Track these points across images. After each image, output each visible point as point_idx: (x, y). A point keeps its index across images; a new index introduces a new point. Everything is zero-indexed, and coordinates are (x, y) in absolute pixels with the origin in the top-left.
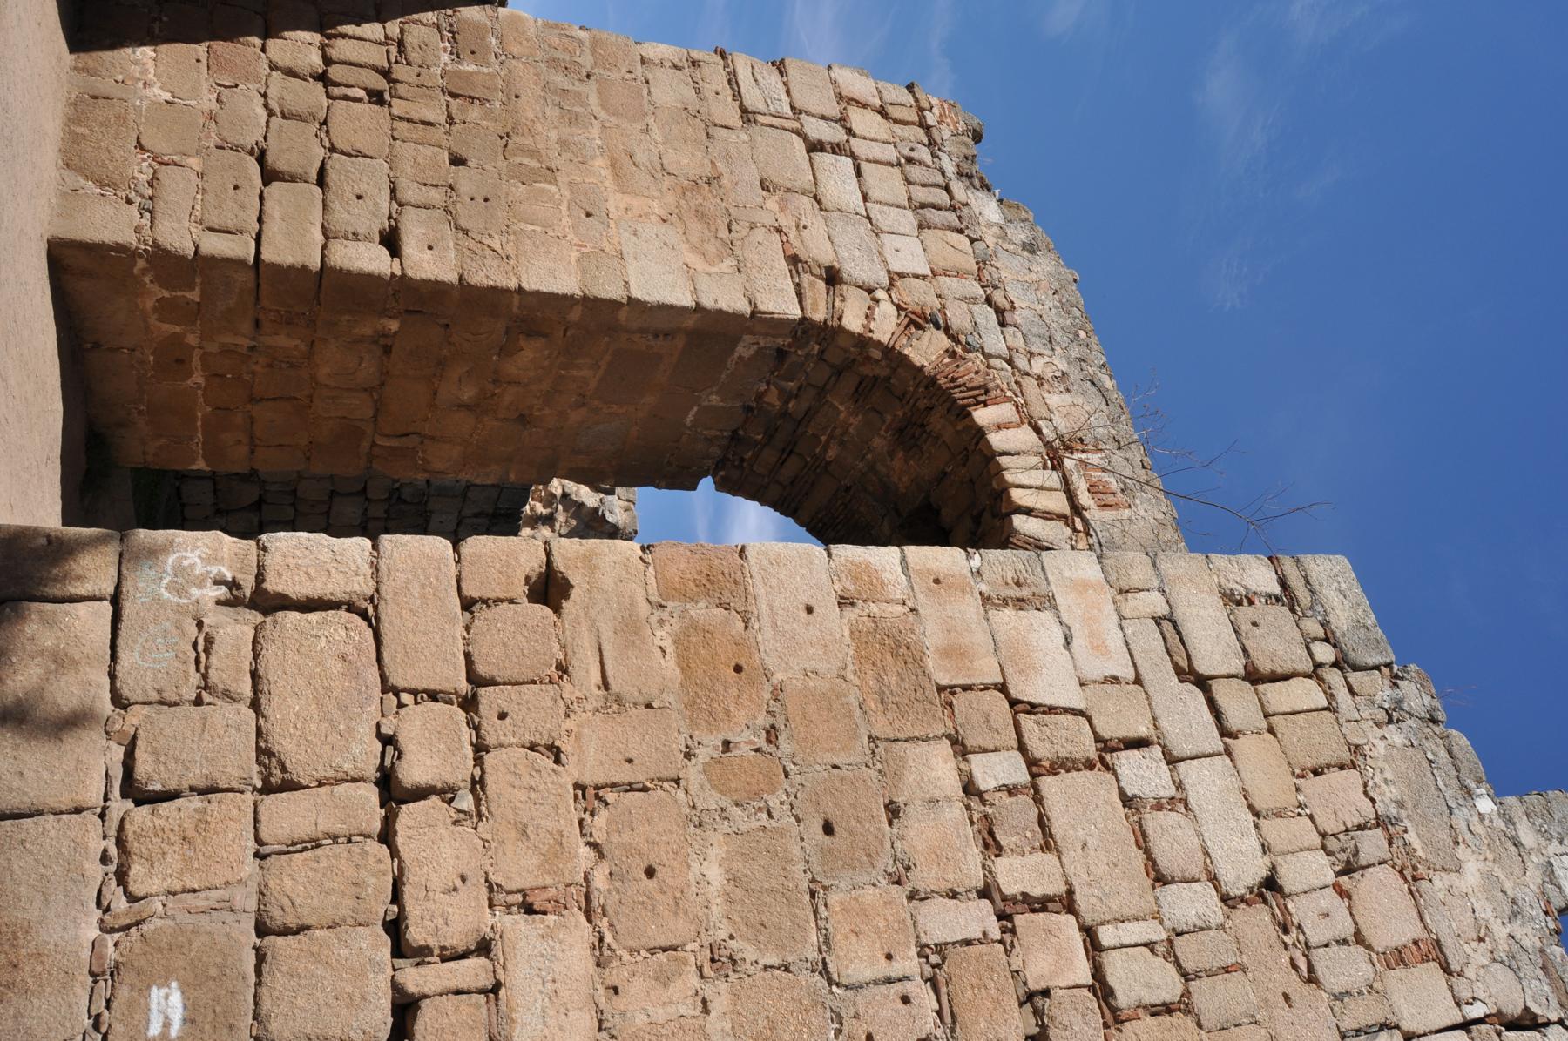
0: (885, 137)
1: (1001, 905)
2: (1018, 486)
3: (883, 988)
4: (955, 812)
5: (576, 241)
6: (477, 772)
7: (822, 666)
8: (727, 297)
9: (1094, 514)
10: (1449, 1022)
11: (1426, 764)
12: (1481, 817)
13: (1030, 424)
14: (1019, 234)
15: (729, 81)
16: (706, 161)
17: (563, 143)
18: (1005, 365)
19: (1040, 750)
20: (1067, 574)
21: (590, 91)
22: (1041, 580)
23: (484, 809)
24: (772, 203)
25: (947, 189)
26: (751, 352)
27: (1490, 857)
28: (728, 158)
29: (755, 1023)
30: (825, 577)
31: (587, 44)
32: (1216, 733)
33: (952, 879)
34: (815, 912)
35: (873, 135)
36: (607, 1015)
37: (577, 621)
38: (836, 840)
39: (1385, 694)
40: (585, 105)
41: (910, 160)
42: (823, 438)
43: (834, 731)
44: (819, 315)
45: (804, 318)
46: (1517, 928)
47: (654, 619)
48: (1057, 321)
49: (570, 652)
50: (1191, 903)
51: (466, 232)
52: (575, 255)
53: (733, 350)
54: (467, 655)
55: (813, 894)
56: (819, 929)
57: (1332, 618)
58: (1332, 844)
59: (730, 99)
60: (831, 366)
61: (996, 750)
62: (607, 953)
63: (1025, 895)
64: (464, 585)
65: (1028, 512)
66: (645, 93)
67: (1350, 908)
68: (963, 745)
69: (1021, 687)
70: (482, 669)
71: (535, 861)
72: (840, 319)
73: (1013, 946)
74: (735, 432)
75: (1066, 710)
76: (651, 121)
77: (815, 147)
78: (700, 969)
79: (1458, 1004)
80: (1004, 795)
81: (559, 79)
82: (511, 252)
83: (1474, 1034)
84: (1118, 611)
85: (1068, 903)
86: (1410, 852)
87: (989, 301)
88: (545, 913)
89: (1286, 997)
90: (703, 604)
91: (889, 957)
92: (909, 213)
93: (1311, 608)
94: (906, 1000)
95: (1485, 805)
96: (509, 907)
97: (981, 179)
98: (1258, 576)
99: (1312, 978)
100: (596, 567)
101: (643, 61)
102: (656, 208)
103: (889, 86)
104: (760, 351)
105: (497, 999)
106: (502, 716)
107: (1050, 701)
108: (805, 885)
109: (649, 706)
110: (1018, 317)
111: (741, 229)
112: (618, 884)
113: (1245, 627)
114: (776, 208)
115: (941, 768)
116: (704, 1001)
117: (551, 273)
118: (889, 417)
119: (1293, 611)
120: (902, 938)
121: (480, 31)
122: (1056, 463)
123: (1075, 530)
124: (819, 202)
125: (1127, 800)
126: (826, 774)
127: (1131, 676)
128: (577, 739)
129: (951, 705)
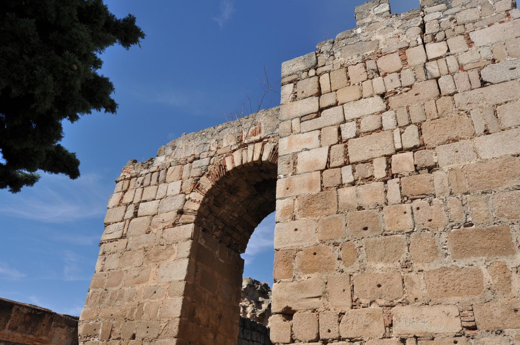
0: (133, 192)
1: (389, 177)
2: (253, 158)
3: (415, 215)
4: (361, 189)
5: (164, 297)
6: (347, 340)
7: (314, 227)
8: (186, 247)
9: (262, 135)
10: (423, 49)
11: (346, 46)
12: (362, 32)
13: (233, 152)
14: (169, 151)
15: (111, 242)
16: (139, 251)
17: (130, 300)
18: (213, 159)
19: (341, 161)
20: (286, 148)
21: (111, 290)
22: (288, 156)
23: (359, 339)
24: (155, 231)
25: (152, 173)
26: (203, 240)
27: (374, 31)
28: (138, 244)
29: (426, 256)
30: (286, 224)
31: (94, 290)
32: (336, 107)
33: (381, 191)
34: (391, 234)
35: (133, 196)
36: (424, 302)
37: (299, 305)
38: (369, 227)
39: (325, 56)
40: (116, 292)
41: (142, 184)
42: (231, 217)
43: (335, 225)
44: (193, 218)
45: (194, 223)
46: (396, 26)
47: (298, 280)
48: (198, 141)
49: (309, 308)
50: (388, 120)
51: (159, 335)
52: (169, 298)
53: (202, 246)
54: (309, 342)
55: (386, 235)
56: (397, 234)
57: (302, 69)
58: (371, 76)
59: (117, 242)
60: (209, 214)
61: (341, 175)
62: (404, 301)
63: (386, 170)
64: (286, 342)
65: (261, 155)
66: (113, 271)
67: (390, 73)
68: (340, 185)
69: (321, 165)
70: (314, 337)
71: (376, 323)
72: (195, 211)
73: (401, 175)
74: (227, 246)
75: (329, 152)
76: (123, 269)
77: (136, 215)
78: (409, 272)
79: (418, 45)
80: (355, 173)
81: (107, 300)
82: (167, 320)
83: (426, 42)
84: (298, 133)
85: (388, 157)
86: (373, 54)
87: (191, 162)
88: (392, 320)
89: (416, 95)
90: (294, 264)
91: (405, 213)
92: (160, 186)
93: (298, 75)
94: (418, 209)
95: (359, 31)
96: (390, 332)
97: (149, 161)
98: (287, 90)
99: (411, 87)
100: (281, 298)
101: (102, 271)
102: (154, 269)
103: (116, 189)
104: (203, 237)
105: (419, 337)
106: (329, 331)
107: (326, 157)
108: (383, 237)
109: (326, 283)
110: (197, 154)
111: (163, 241)
112: (383, 296)
113: (304, 95)
114: (156, 229)
115: (347, 193)
116: (419, 271)
117: (175, 306)
118: (227, 196)
119: (299, 80)
120: (399, 208)
121: (87, 327)
122: (245, 146)
123: (267, 141)
124: (155, 215)
125: (357, 136)
126: (349, 228)
127: (318, 131)
128: (337, 307)
129: (327, 188)
